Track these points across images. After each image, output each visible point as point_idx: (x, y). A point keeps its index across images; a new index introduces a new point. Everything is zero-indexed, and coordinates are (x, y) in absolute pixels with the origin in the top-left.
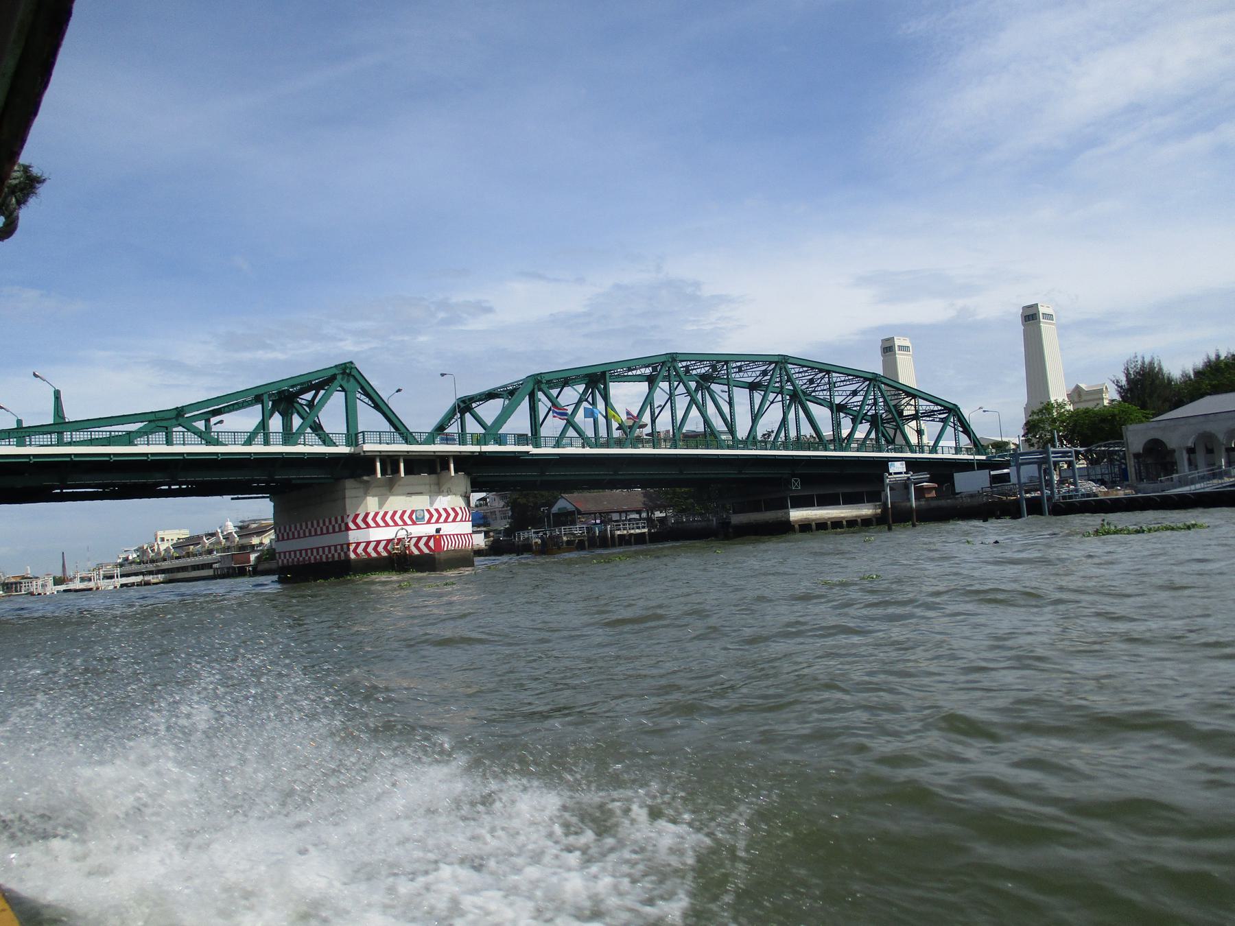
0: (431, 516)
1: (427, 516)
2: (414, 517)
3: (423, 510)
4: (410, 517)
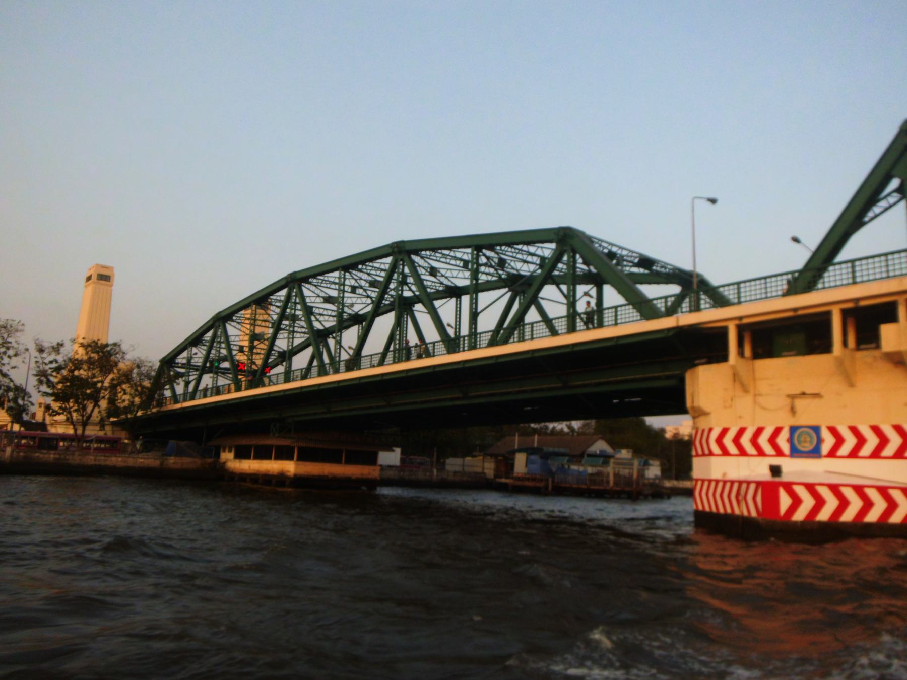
1: (829, 441)
3: (816, 429)
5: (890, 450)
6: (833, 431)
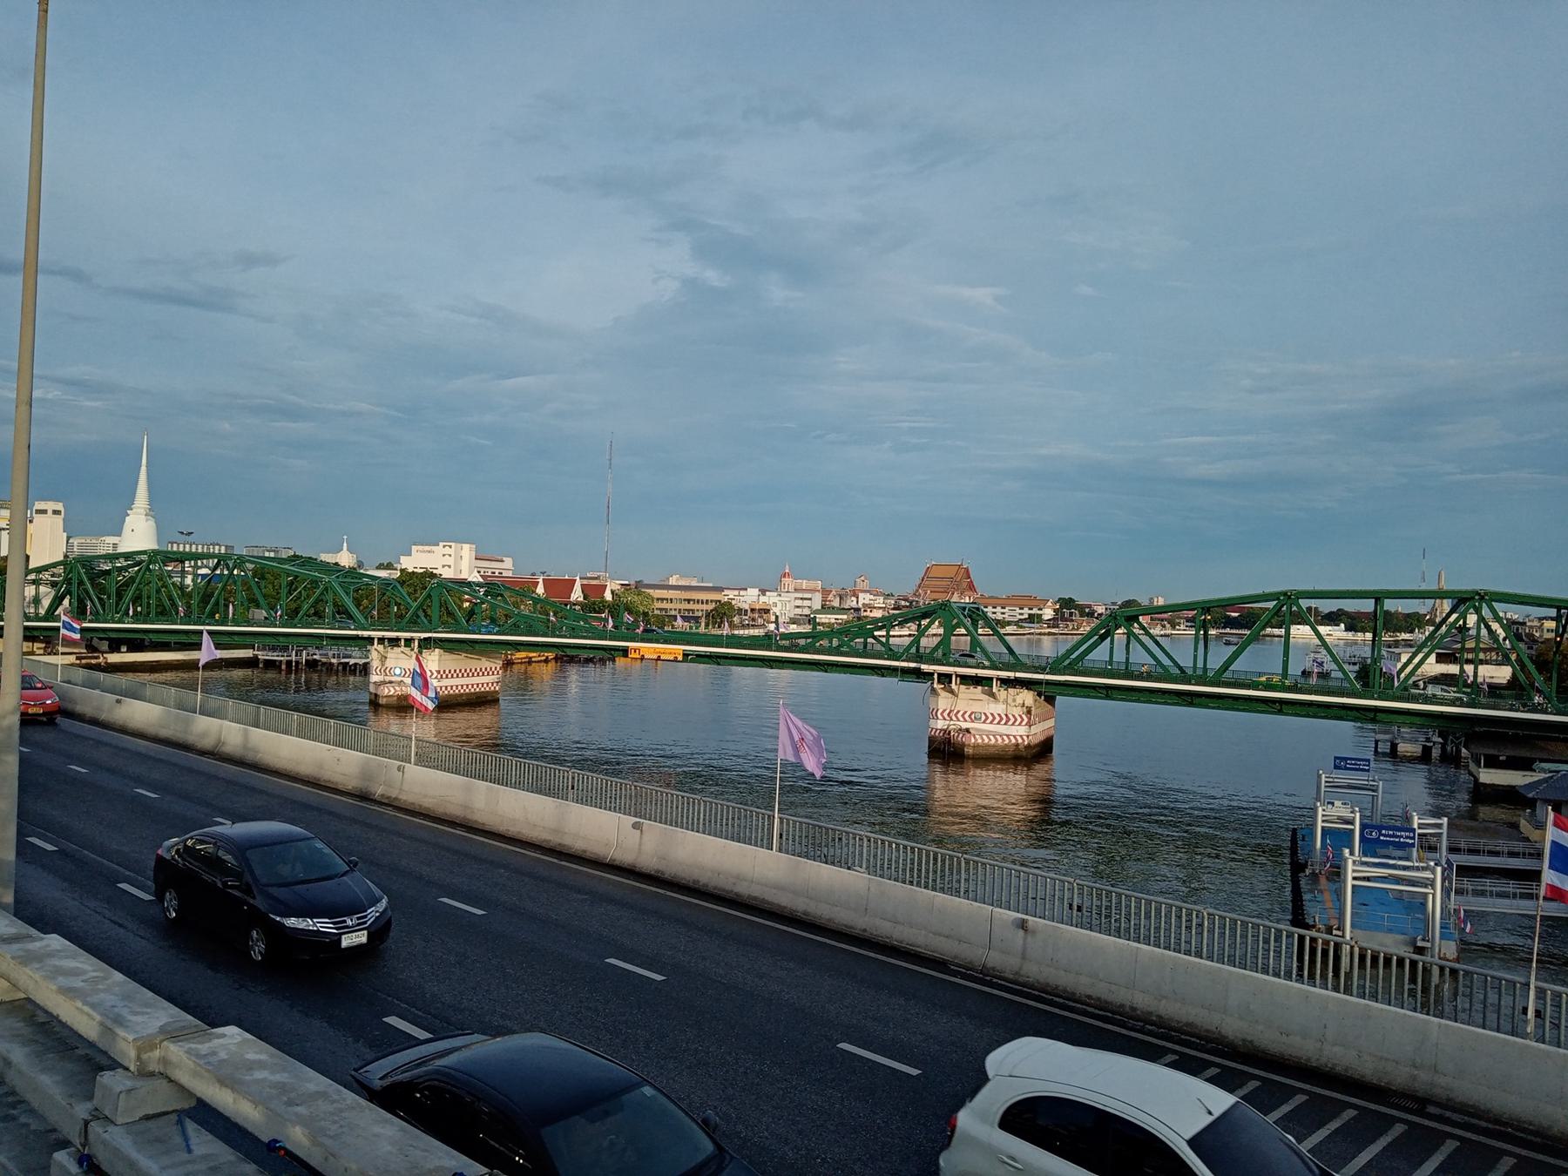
0: (987, 718)
1: (983, 717)
2: (973, 717)
4: (970, 716)
5: (1024, 723)
6: (985, 714)
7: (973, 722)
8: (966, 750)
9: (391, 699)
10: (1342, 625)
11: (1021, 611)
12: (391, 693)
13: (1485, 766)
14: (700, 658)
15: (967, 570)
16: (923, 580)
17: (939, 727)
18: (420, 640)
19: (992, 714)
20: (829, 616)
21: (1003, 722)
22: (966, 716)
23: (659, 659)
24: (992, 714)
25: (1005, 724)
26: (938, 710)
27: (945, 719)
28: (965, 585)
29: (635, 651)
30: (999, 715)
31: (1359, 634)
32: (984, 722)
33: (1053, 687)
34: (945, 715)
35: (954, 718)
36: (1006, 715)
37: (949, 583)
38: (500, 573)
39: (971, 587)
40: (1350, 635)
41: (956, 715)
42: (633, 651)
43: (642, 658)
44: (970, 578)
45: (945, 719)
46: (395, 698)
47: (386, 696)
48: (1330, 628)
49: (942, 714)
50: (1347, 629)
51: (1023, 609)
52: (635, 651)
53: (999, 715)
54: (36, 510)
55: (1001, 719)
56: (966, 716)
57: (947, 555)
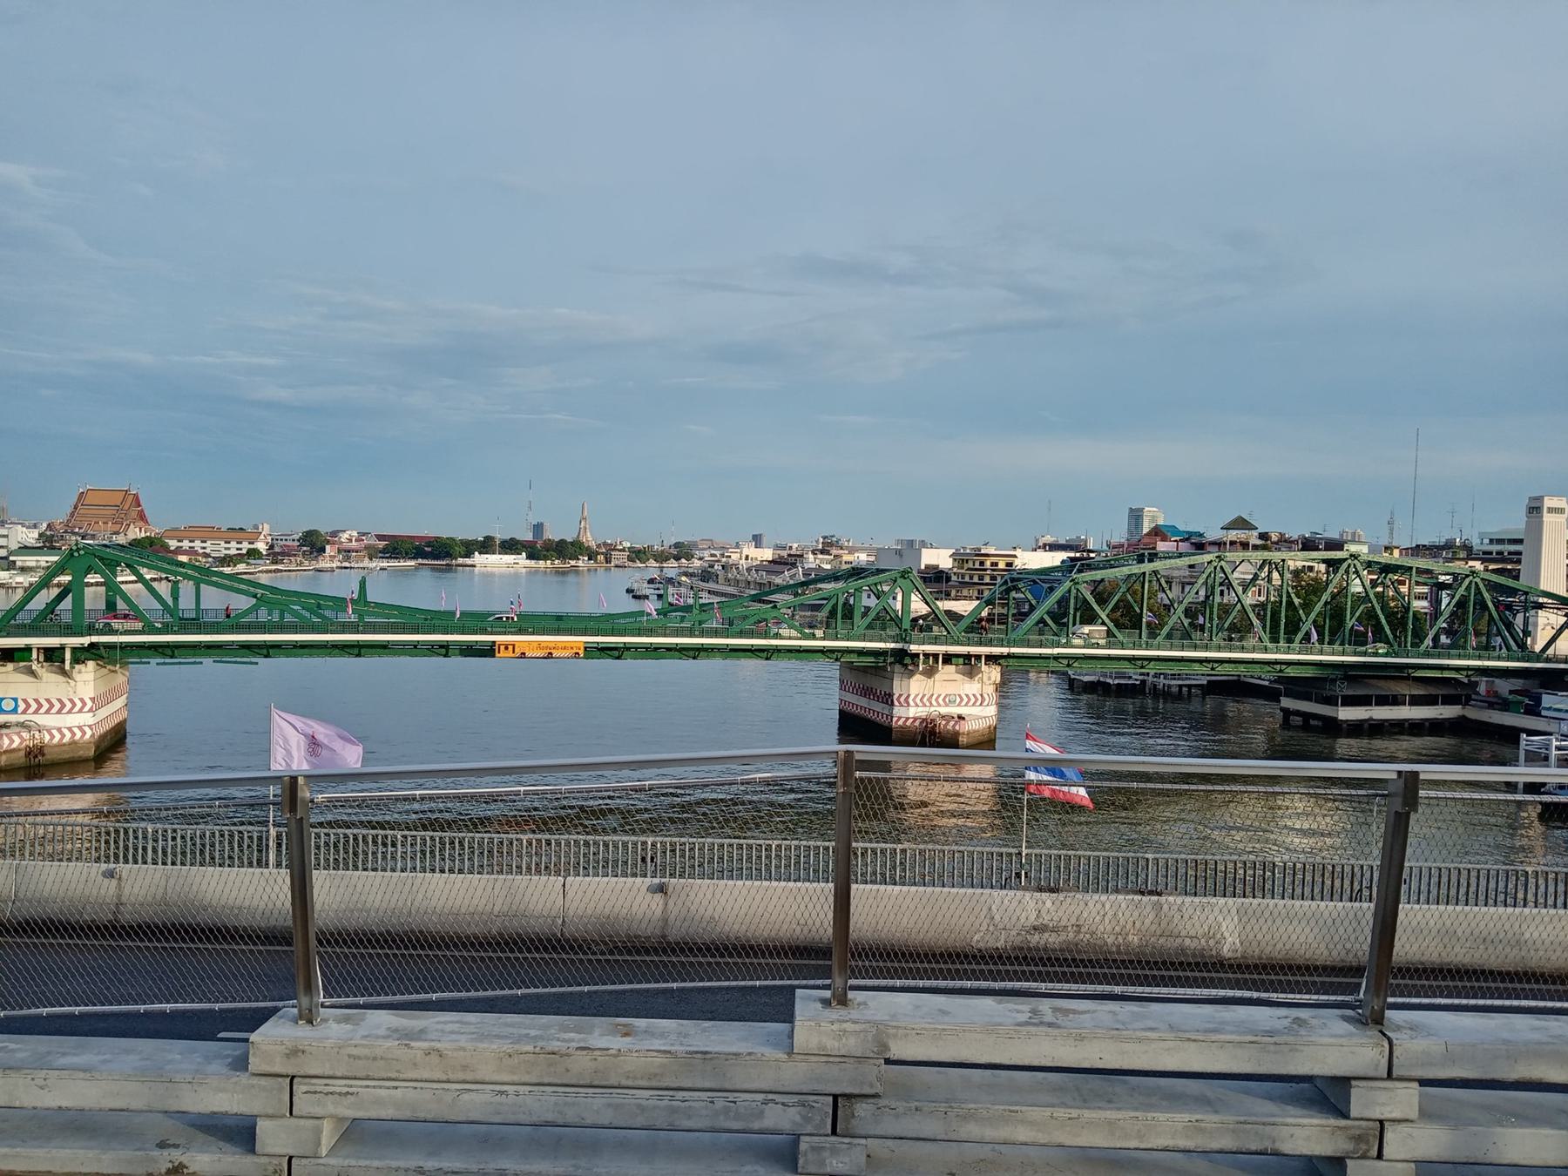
1: (958, 700)
4: (944, 700)
7: (947, 705)
8: (960, 739)
9: (13, 755)
10: (524, 554)
11: (227, 545)
12: (15, 746)
13: (1342, 705)
14: (605, 651)
15: (136, 497)
16: (76, 508)
17: (911, 715)
18: (74, 650)
19: (967, 695)
20: (39, 558)
21: (978, 703)
22: (940, 700)
23: (550, 656)
24: (967, 695)
25: (981, 705)
26: (909, 696)
27: (917, 705)
28: (134, 514)
29: (506, 648)
30: (974, 695)
31: (541, 562)
32: (959, 705)
33: (1164, 663)
34: (918, 700)
35: (934, 703)
36: (982, 695)
37: (115, 512)
38: (992, 564)
39: (142, 517)
40: (532, 563)
41: (914, 700)
42: (502, 648)
43: (523, 655)
44: (139, 506)
45: (917, 705)
46: (22, 753)
47: (5, 752)
48: (514, 557)
49: (914, 700)
50: (530, 557)
51: (193, 541)
52: (506, 648)
53: (974, 695)
54: (1549, 508)
55: (977, 699)
56: (940, 700)
57: (108, 479)
